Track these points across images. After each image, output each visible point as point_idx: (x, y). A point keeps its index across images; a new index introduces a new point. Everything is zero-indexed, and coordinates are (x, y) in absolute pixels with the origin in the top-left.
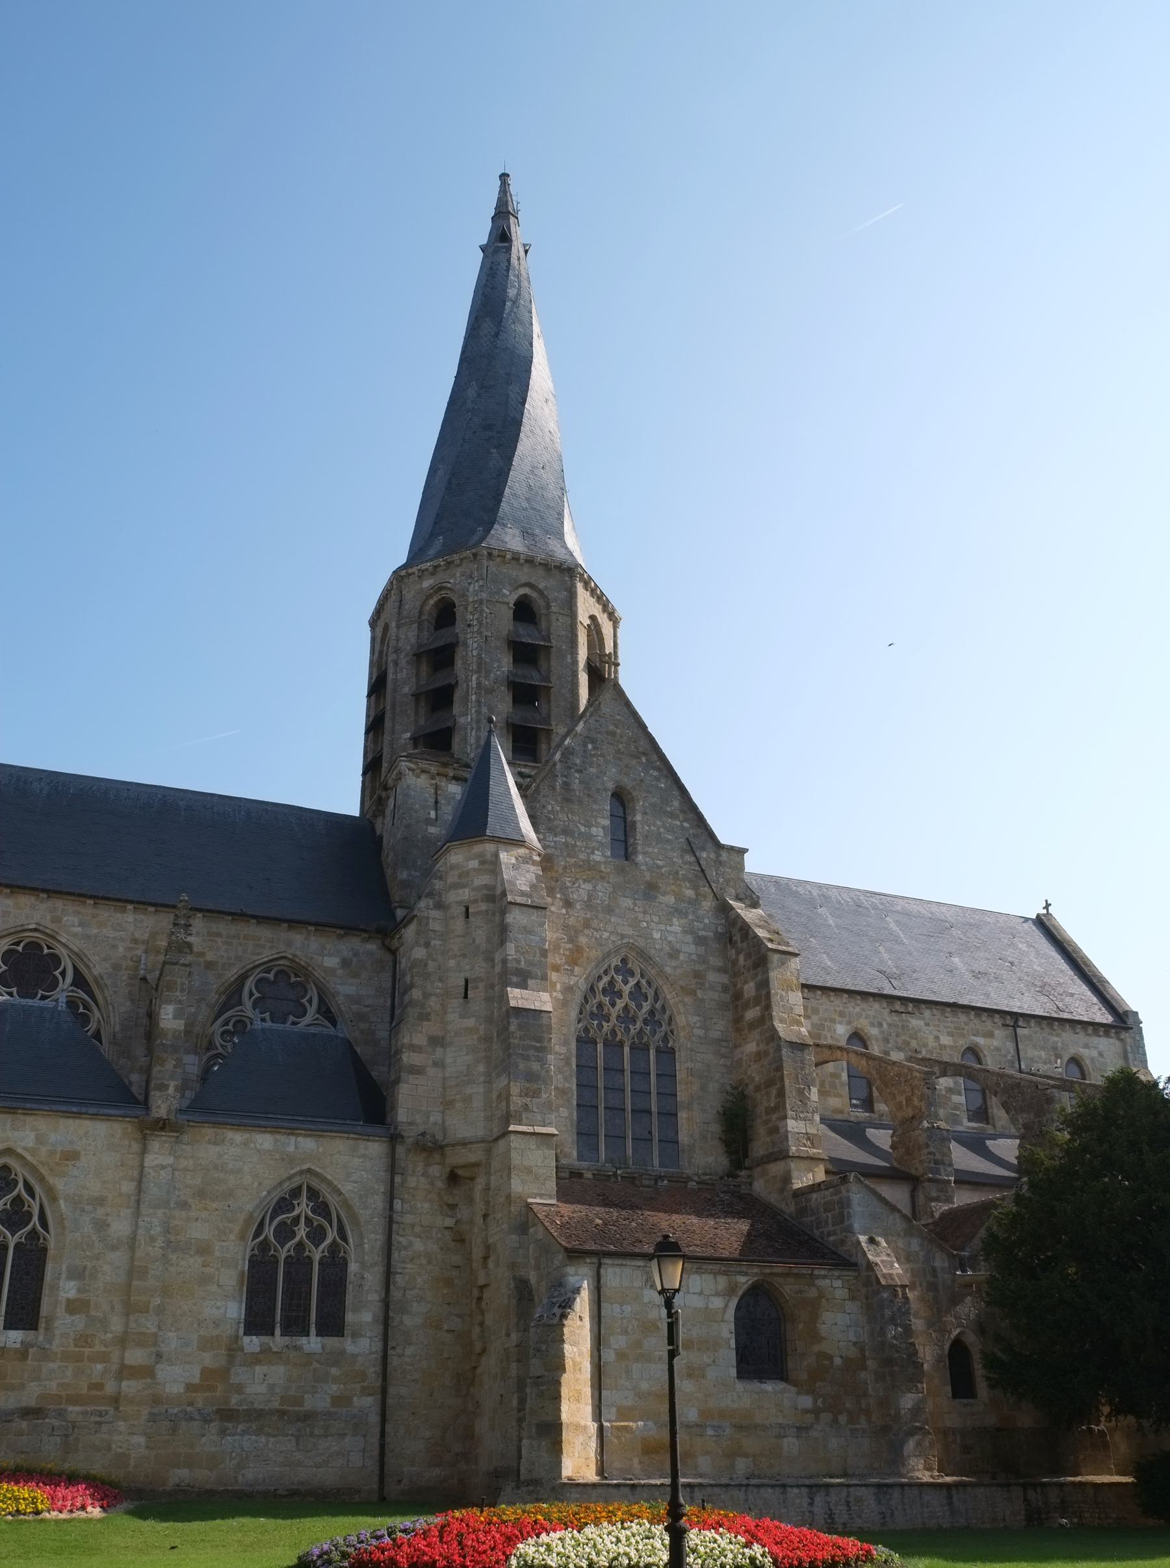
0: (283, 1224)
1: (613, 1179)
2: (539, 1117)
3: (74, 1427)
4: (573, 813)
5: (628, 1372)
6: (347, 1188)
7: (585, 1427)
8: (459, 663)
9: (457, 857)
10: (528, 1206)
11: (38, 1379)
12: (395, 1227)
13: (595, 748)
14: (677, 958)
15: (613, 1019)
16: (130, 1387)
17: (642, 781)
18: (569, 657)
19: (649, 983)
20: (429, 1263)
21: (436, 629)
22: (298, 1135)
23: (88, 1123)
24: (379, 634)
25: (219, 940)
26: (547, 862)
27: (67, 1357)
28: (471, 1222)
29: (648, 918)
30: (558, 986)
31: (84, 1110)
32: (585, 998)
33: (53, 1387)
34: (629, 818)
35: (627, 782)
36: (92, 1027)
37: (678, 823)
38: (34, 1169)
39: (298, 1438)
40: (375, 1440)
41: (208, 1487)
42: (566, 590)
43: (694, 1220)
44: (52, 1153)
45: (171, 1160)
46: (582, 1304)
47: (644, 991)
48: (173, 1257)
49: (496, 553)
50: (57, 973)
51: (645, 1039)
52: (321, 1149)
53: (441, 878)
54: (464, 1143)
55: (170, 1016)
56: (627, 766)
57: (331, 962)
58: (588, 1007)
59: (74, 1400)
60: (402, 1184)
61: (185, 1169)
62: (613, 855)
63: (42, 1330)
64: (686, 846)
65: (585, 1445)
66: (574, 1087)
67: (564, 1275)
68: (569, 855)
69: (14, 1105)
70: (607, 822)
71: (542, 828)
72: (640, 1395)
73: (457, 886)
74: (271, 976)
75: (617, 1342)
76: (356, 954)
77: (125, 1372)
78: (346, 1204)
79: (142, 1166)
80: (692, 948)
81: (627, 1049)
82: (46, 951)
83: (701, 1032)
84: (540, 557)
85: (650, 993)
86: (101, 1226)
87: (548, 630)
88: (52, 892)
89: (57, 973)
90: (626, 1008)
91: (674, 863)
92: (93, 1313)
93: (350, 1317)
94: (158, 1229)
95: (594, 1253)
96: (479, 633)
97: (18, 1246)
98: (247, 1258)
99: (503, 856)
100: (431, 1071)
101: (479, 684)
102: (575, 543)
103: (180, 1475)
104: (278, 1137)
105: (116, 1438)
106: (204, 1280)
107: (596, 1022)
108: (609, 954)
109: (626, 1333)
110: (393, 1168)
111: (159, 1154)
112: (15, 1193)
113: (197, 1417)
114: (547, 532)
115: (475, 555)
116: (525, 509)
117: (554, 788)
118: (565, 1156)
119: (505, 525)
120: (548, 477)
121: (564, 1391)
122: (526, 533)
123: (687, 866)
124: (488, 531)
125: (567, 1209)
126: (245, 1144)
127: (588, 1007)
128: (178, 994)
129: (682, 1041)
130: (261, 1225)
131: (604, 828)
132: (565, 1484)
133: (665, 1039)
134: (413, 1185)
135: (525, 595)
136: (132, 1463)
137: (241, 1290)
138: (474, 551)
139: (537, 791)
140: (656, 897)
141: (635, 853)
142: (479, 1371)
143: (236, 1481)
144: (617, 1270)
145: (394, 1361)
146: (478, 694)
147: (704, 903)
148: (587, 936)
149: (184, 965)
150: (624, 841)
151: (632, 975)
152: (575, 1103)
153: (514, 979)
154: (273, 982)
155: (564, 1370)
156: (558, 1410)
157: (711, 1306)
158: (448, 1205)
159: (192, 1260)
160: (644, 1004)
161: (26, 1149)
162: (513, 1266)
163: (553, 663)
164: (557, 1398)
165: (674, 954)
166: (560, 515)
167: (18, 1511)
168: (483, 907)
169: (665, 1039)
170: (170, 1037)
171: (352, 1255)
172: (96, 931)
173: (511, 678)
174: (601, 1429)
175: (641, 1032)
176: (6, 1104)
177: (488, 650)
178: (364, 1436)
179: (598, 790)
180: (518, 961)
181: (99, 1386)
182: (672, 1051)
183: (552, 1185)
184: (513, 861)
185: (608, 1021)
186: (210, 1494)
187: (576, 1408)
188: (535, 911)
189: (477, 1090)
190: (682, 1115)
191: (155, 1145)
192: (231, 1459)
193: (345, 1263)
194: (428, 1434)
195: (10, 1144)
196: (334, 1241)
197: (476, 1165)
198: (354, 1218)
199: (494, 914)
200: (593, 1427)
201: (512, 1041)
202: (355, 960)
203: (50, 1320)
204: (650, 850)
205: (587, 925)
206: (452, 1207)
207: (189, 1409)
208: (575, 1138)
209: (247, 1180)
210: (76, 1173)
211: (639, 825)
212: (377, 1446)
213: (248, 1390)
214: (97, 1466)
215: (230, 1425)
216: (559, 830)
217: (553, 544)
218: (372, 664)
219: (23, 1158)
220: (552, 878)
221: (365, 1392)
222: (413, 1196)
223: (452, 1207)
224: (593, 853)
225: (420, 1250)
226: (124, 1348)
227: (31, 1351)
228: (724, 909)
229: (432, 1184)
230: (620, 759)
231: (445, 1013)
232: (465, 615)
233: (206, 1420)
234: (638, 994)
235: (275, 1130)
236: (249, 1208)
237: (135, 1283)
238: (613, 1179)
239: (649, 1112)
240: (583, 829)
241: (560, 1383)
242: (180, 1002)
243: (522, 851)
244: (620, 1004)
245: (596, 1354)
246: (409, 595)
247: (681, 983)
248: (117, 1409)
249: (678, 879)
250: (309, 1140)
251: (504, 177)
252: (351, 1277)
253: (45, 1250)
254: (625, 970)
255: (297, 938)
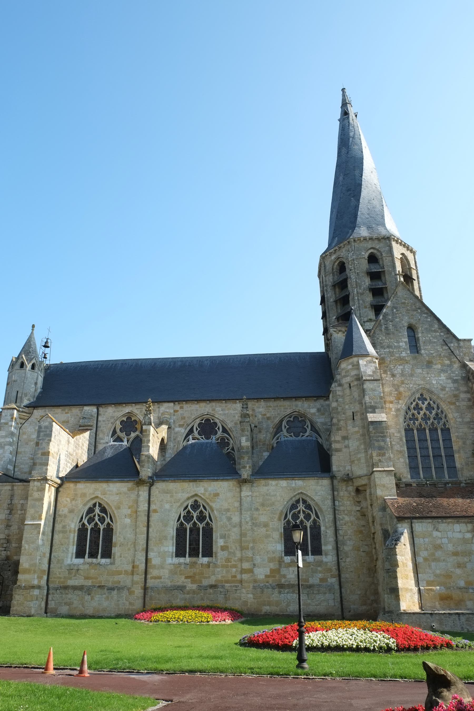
0: (294, 514)
1: (426, 486)
2: (386, 464)
3: (228, 591)
4: (391, 339)
5: (430, 566)
6: (316, 498)
7: (411, 590)
8: (349, 286)
9: (345, 365)
10: (385, 500)
11: (214, 574)
12: (336, 512)
13: (397, 311)
14: (445, 390)
15: (420, 419)
16: (245, 577)
17: (419, 320)
18: (393, 273)
19: (434, 402)
20: (352, 525)
21: (340, 274)
22: (295, 480)
23: (221, 483)
24: (321, 280)
25: (271, 408)
26: (382, 361)
27: (223, 566)
28: (367, 508)
29: (429, 376)
30: (393, 409)
31: (219, 478)
32: (406, 412)
33: (219, 577)
34: (416, 336)
35: (413, 322)
36: (231, 446)
37: (438, 334)
38: (205, 501)
39: (308, 594)
40: (338, 595)
41: (277, 613)
42: (388, 246)
43: (460, 500)
44: (210, 494)
45: (250, 493)
46: (405, 539)
47: (432, 406)
48: (256, 529)
49: (356, 239)
50: (216, 429)
51: (435, 426)
52: (305, 484)
53: (339, 374)
54: (360, 477)
55: (244, 441)
56: (412, 315)
57: (313, 411)
58: (408, 416)
59: (227, 582)
60: (338, 495)
61: (256, 496)
62: (411, 352)
63: (214, 557)
64: (443, 343)
65: (412, 597)
66: (406, 449)
67: (397, 528)
68: (391, 356)
69: (196, 479)
70: (407, 340)
71: (378, 347)
72: (436, 576)
73: (345, 376)
74: (292, 419)
75: (423, 554)
76: (322, 406)
77: (243, 571)
78: (317, 504)
79: (241, 496)
80: (452, 385)
81: (427, 431)
82: (212, 421)
83: (460, 420)
84: (375, 236)
85: (435, 406)
86: (229, 519)
87: (383, 264)
88: (211, 400)
89: (216, 429)
90: (425, 414)
91: (438, 351)
92: (230, 550)
93: (323, 548)
94: (249, 519)
95: (409, 517)
96: (355, 272)
97: (203, 528)
98: (282, 527)
99: (361, 362)
100: (344, 450)
101: (357, 292)
102: (391, 226)
103: (266, 609)
104: (288, 481)
105: (242, 595)
106: (267, 536)
107: (412, 422)
108: (414, 393)
109: (427, 550)
110: (333, 489)
111: (246, 491)
112: (200, 509)
113: (270, 587)
114: (378, 225)
115: (349, 242)
116: (368, 218)
117: (381, 330)
118: (405, 478)
119: (360, 227)
120: (375, 202)
121: (399, 575)
122: (369, 228)
123: (445, 351)
124: (353, 231)
125: (401, 500)
126: (277, 485)
127: (408, 416)
128: (246, 432)
129: (452, 425)
130: (286, 515)
131: (405, 342)
132: (402, 613)
133: (444, 424)
134: (342, 495)
135: (372, 253)
136: (249, 604)
137: (281, 539)
138: (348, 240)
139: (374, 333)
140: (432, 367)
141: (420, 350)
142: (377, 567)
143: (287, 611)
144: (420, 524)
145: (342, 564)
146: (358, 296)
147: (454, 365)
148: (403, 387)
149: (247, 422)
150: (414, 346)
151: (426, 400)
152: (407, 456)
153: (370, 410)
154: (293, 421)
155: (398, 566)
156: (397, 583)
157: (466, 537)
158: (357, 501)
159: (262, 529)
160: (433, 411)
161: (201, 494)
162: (381, 524)
163: (387, 277)
164: (396, 578)
165: (443, 389)
166: (383, 216)
167: (201, 621)
168: (356, 383)
169: (444, 424)
170: (245, 449)
171: (322, 524)
172: (227, 412)
173: (370, 287)
174: (419, 590)
175: (433, 423)
176: (193, 479)
177: (363, 278)
178: (334, 594)
179: (400, 327)
180: (371, 403)
181: (235, 577)
182: (448, 430)
183: (394, 490)
184: (365, 363)
185: (418, 421)
186: (278, 615)
187: (406, 580)
188: (375, 381)
189: (362, 455)
190: (456, 456)
191: (244, 488)
192: (284, 602)
193: (319, 527)
194: (359, 593)
195: (196, 493)
196: (314, 519)
197: (365, 485)
198: (321, 510)
199: (360, 385)
200: (415, 589)
201: (371, 435)
202: (322, 408)
203: (216, 554)
204: (427, 347)
205: (403, 383)
206: (359, 502)
207: (267, 584)
208: (409, 470)
209: (279, 498)
210: (219, 501)
211: (420, 338)
212: (339, 597)
213: (288, 577)
214: (237, 606)
215: (282, 590)
216: (385, 347)
217: (381, 229)
218: (321, 291)
219: (201, 497)
220: (385, 366)
221: (332, 576)
222: (343, 499)
223: (359, 502)
224: (401, 353)
225: (348, 519)
226: (242, 562)
227: (211, 564)
228: (464, 366)
229: (350, 494)
230: (408, 313)
231: (347, 426)
232: (349, 266)
233: (273, 588)
234: (429, 407)
235: (287, 478)
236: (281, 508)
237: (243, 539)
238: (426, 486)
239: (441, 456)
240: (396, 344)
241: (396, 572)
242: (247, 436)
243: (369, 358)
244: (422, 413)
245: (414, 559)
246: (327, 263)
247: (449, 400)
248: (242, 584)
249: (441, 357)
250: (300, 481)
251: (343, 90)
252: (322, 532)
253: (212, 528)
254: (422, 398)
255: (299, 403)
